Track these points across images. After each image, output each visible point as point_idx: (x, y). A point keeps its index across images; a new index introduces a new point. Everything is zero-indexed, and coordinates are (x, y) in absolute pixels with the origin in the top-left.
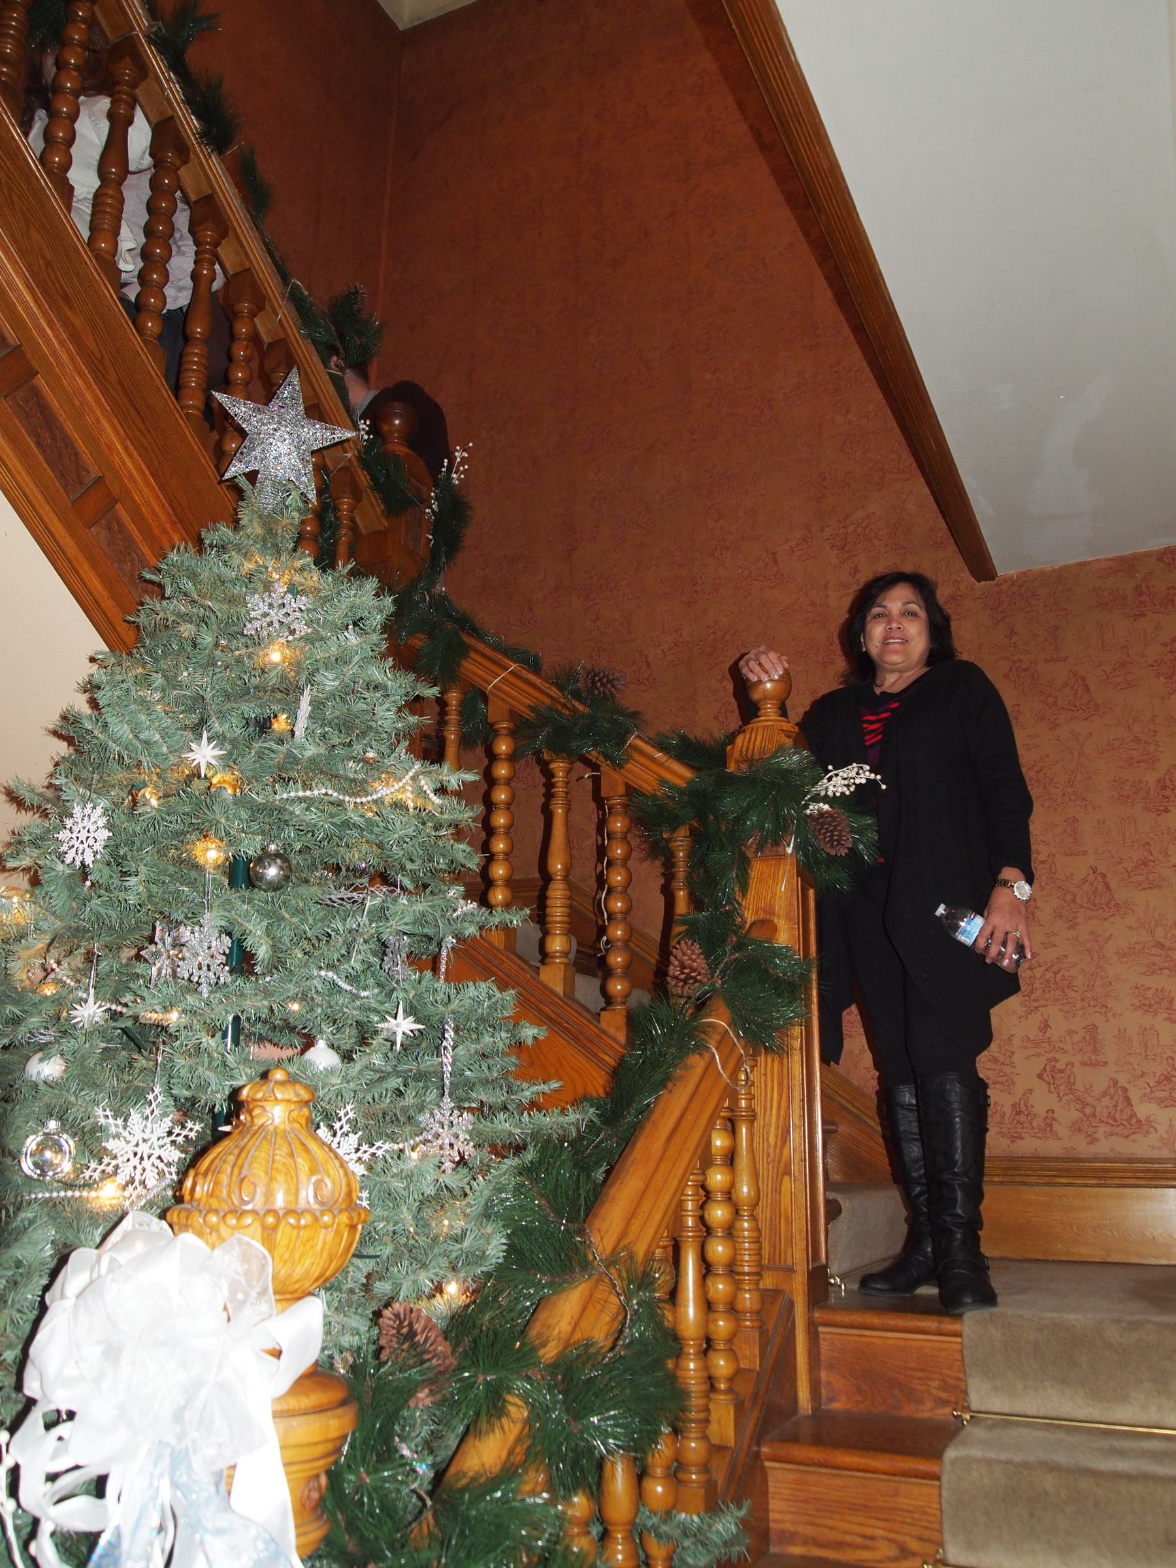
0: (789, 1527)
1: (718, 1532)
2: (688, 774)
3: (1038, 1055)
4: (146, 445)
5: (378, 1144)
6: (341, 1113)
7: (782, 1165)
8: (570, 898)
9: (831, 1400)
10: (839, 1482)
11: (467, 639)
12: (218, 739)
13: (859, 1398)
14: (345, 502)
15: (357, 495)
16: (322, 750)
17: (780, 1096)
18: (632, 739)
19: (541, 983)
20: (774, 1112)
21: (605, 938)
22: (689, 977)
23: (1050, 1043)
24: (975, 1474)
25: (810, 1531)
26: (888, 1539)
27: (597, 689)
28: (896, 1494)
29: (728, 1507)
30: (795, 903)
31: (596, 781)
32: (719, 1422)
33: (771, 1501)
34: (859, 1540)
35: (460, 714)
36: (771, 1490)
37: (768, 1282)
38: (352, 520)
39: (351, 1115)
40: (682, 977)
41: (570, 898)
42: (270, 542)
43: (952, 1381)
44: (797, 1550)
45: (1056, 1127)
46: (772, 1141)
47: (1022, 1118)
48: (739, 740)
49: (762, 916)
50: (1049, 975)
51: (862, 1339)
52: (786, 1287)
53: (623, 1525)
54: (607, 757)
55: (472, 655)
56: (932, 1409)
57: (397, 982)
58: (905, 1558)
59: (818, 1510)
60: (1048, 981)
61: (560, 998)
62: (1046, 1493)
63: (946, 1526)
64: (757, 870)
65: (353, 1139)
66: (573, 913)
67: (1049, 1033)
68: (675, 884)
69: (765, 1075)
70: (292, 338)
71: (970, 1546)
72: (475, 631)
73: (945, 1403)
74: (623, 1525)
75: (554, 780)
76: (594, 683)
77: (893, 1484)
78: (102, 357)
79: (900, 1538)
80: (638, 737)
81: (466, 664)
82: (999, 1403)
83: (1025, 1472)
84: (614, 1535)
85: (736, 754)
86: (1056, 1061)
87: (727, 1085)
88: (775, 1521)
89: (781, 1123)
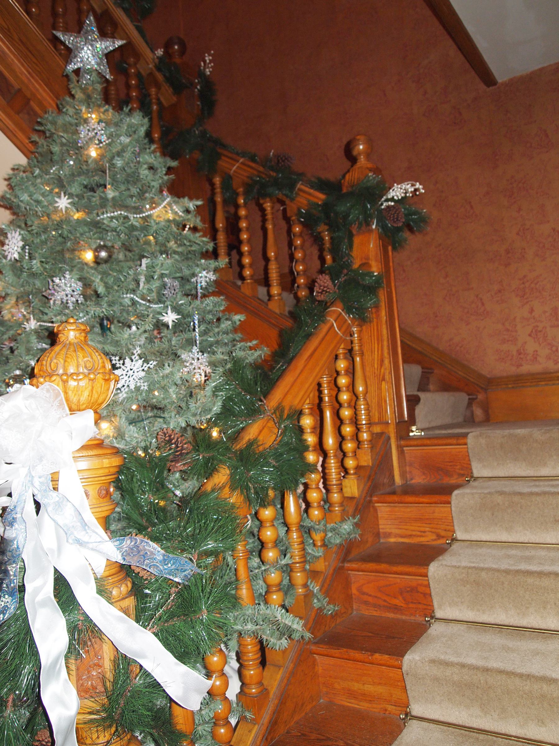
0: (388, 530)
1: (345, 529)
2: (322, 196)
3: (528, 325)
4: (39, 70)
5: (151, 363)
6: (135, 352)
7: (381, 376)
8: (279, 268)
9: (412, 479)
10: (408, 510)
11: (220, 151)
12: (71, 196)
13: (424, 477)
14: (153, 91)
15: (158, 86)
16: (117, 194)
17: (378, 344)
18: (299, 185)
19: (270, 310)
20: (376, 353)
21: (296, 285)
22: (323, 291)
23: (534, 319)
24: (466, 499)
25: (397, 531)
26: (431, 532)
27: (280, 163)
28: (434, 512)
29: (349, 519)
30: (379, 253)
31: (285, 211)
32: (351, 487)
33: (380, 521)
34: (419, 533)
35: (222, 188)
36: (379, 516)
37: (377, 429)
38: (158, 99)
39: (139, 352)
40: (320, 291)
41: (279, 268)
42: (88, 101)
43: (465, 465)
44: (392, 540)
45: (538, 358)
46: (376, 366)
47: (522, 356)
48: (347, 177)
49: (364, 261)
50: (533, 285)
51: (424, 451)
52: (386, 431)
53: (295, 524)
54: (287, 196)
55: (223, 158)
56: (457, 479)
57: (167, 298)
58: (439, 539)
59: (400, 522)
60: (532, 288)
61: (279, 316)
62: (498, 504)
63: (455, 524)
64: (357, 241)
65: (140, 362)
66: (282, 276)
67: (533, 314)
68: (325, 253)
69: (371, 336)
70: (111, 8)
71: (466, 531)
72: (224, 146)
73: (463, 475)
74: (295, 524)
75: (266, 212)
76: (278, 161)
77: (433, 508)
78: (8, 27)
79: (438, 531)
80: (302, 184)
81: (220, 162)
82: (486, 473)
83: (489, 496)
84: (291, 529)
85: (346, 184)
86: (537, 326)
87: (341, 337)
88: (383, 529)
89: (379, 358)
